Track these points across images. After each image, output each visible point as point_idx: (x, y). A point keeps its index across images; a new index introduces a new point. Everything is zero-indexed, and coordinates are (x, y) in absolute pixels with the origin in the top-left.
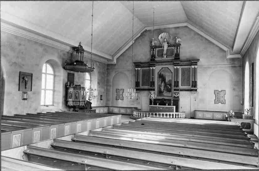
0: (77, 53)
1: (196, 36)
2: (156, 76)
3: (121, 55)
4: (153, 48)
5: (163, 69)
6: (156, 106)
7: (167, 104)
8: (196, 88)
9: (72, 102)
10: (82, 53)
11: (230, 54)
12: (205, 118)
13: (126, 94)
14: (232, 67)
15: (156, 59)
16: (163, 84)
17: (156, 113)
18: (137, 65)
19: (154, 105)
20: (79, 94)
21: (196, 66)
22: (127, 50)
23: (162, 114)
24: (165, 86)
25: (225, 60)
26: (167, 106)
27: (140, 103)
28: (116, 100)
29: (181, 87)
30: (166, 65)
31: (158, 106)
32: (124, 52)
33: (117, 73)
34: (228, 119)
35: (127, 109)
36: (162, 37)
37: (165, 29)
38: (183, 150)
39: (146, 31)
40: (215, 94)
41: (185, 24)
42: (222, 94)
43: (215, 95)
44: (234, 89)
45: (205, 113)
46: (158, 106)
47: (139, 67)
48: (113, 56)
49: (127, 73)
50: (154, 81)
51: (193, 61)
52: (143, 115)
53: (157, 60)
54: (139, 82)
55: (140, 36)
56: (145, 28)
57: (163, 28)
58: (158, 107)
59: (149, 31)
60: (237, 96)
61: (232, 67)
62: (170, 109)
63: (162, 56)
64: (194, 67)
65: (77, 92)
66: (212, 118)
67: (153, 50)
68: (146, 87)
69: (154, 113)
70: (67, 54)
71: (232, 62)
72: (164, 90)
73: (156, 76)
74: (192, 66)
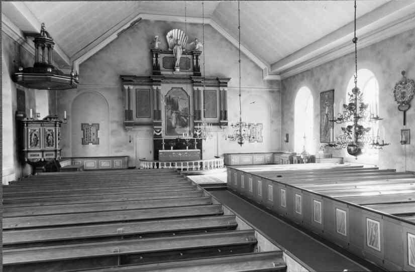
0: (40, 48)
1: (224, 43)
2: (163, 103)
3: (89, 59)
4: (153, 53)
5: (175, 90)
6: (185, 150)
7: (172, 147)
8: (226, 121)
9: (54, 153)
10: (46, 48)
11: (269, 75)
12: (242, 163)
13: (102, 135)
14: (270, 91)
15: (162, 73)
16: (174, 115)
17: (197, 161)
18: (125, 79)
19: (165, 149)
20: (52, 136)
21: (226, 89)
22: (101, 50)
23: (169, 166)
24: (178, 117)
25: (262, 82)
26: (172, 150)
27: (135, 148)
28: (83, 144)
29: (136, 120)
30: (180, 83)
31: (172, 150)
32: (97, 54)
33: (80, 92)
34: (304, 161)
35: (115, 161)
36: (171, 37)
37: (174, 23)
38: (138, 225)
39: (140, 20)
40: (82, 129)
41: (207, 21)
42: (93, 130)
43: (82, 132)
44: (272, 122)
45: (242, 156)
46: (172, 150)
47: (200, 86)
48: (72, 58)
49: (105, 94)
50: (160, 109)
51: (221, 82)
52: (210, 166)
53: (166, 74)
54: (132, 111)
55: (128, 28)
56: (138, 15)
57: (172, 20)
58: (187, 152)
59: (146, 21)
60: (276, 130)
61: (270, 91)
62: (195, 154)
63: (173, 68)
64: (197, 89)
65: (49, 130)
66: (251, 163)
67: (157, 57)
68: (145, 120)
69: (188, 163)
70: (14, 44)
71: (270, 86)
72: (176, 124)
73: (163, 103)
74: (153, 86)
